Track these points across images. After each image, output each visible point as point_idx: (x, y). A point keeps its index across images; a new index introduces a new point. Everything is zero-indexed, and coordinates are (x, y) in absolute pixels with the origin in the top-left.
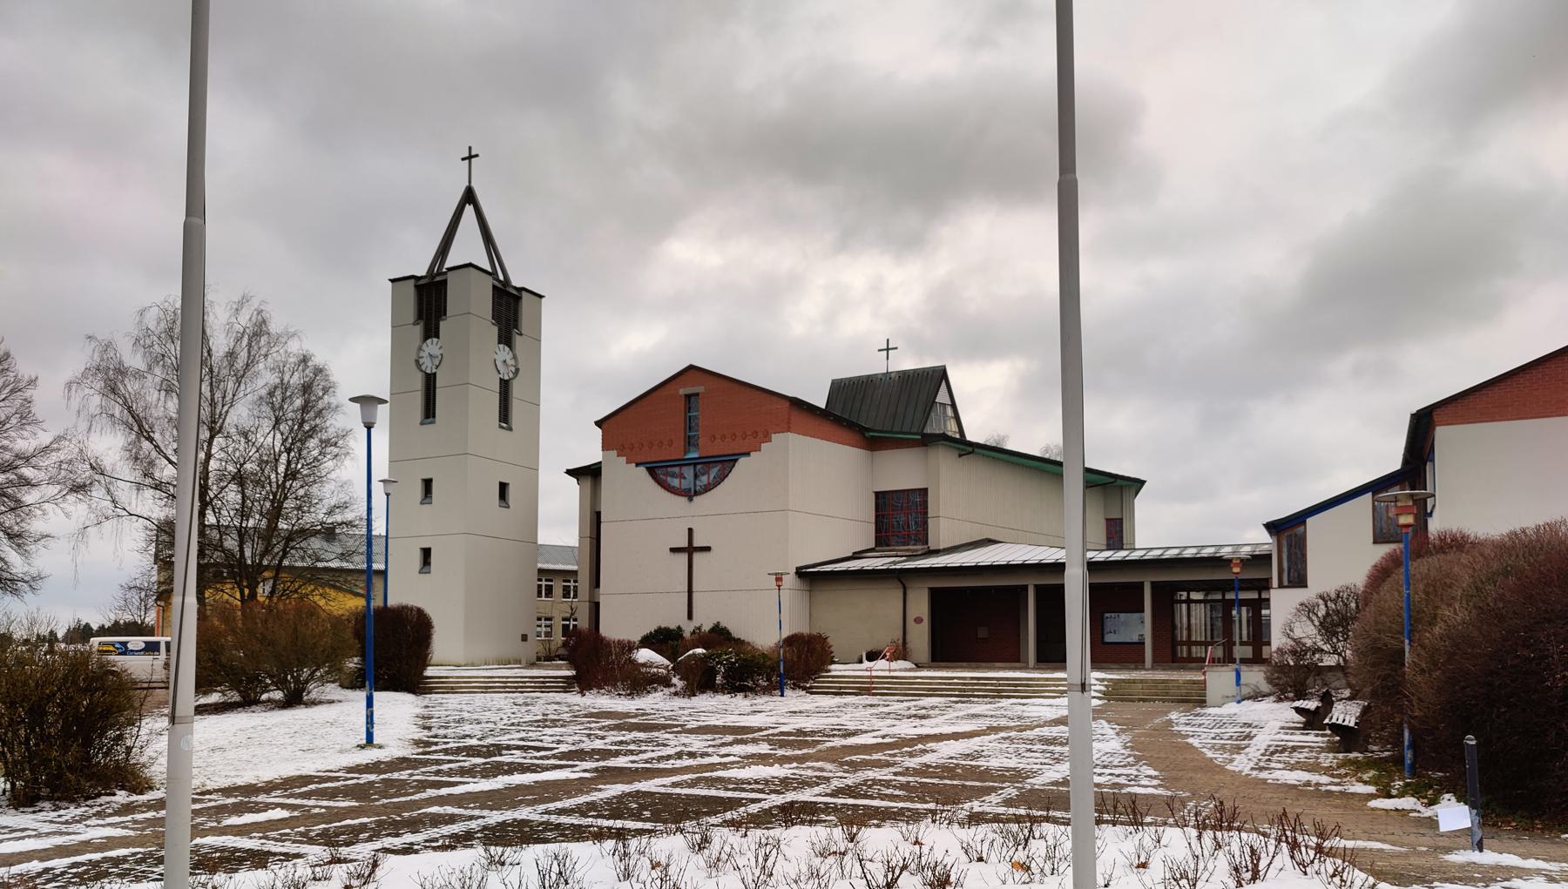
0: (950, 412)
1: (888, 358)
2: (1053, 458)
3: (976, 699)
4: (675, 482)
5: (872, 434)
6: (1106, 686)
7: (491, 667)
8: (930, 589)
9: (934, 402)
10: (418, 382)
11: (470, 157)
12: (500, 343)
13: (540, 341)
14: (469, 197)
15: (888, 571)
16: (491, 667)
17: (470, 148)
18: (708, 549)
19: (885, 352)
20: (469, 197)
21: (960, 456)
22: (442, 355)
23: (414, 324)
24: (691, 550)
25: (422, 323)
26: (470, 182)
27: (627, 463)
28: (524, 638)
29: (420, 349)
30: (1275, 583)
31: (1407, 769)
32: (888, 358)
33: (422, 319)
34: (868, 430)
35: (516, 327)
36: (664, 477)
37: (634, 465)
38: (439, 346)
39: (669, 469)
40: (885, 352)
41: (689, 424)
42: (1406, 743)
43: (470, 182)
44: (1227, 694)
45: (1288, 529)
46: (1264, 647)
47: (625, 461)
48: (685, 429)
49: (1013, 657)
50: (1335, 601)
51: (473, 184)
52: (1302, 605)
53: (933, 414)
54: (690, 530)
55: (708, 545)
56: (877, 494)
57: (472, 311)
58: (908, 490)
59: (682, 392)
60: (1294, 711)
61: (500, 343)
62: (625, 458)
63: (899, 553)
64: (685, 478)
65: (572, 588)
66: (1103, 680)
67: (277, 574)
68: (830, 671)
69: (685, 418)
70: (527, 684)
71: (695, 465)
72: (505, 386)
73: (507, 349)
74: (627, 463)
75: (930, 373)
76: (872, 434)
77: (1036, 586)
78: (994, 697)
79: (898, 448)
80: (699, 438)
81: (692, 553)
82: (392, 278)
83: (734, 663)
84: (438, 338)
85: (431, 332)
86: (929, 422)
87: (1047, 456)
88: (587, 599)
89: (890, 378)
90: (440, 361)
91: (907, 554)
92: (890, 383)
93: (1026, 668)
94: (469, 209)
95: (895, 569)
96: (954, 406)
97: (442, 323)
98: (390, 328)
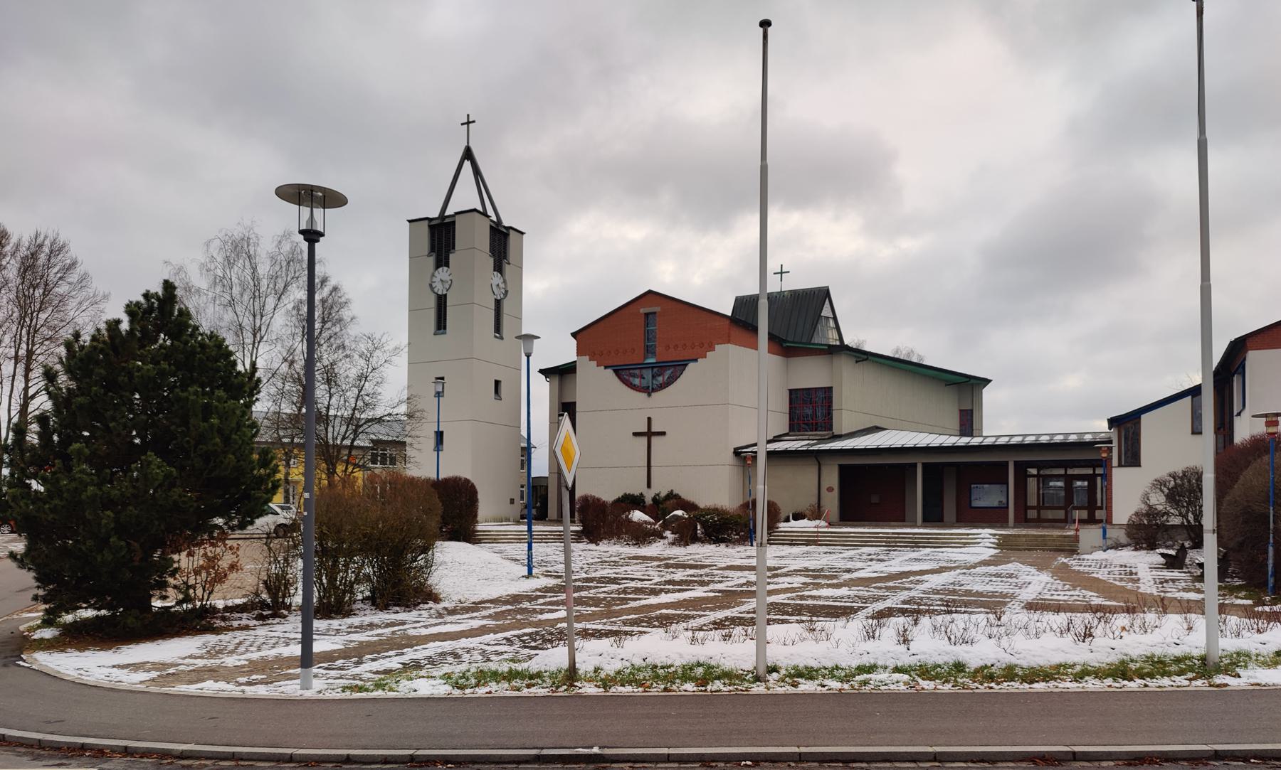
0: (832, 323)
1: (781, 280)
2: (902, 358)
3: (899, 549)
4: (637, 381)
5: (788, 344)
6: (998, 539)
7: (490, 524)
8: (1015, 461)
9: (820, 315)
10: (432, 302)
11: (468, 123)
12: (494, 270)
13: (522, 268)
14: (468, 155)
15: (807, 451)
16: (490, 524)
17: (468, 115)
18: (663, 433)
19: (780, 275)
20: (468, 155)
21: (857, 362)
22: (451, 280)
23: (428, 256)
24: (649, 434)
25: (434, 255)
26: (468, 143)
27: (598, 366)
28: (512, 501)
29: (433, 275)
30: (1115, 462)
31: (1269, 590)
32: (781, 280)
33: (434, 252)
34: (785, 341)
35: (505, 257)
36: (627, 378)
37: (603, 367)
38: (449, 272)
39: (631, 371)
40: (780, 275)
41: (648, 336)
42: (1270, 573)
43: (468, 143)
44: (1094, 545)
45: (1127, 424)
46: (1097, 511)
47: (596, 365)
48: (645, 340)
49: (900, 517)
50: (1181, 479)
51: (470, 145)
52: (1156, 480)
53: (819, 326)
54: (649, 419)
55: (663, 430)
56: (791, 391)
57: (475, 246)
58: (816, 388)
59: (642, 311)
60: (1160, 556)
61: (494, 270)
62: (596, 362)
63: (811, 437)
64: (644, 378)
65: (388, 455)
66: (995, 535)
67: (350, 452)
68: (777, 528)
69: (645, 331)
70: (549, 537)
71: (653, 368)
72: (498, 304)
73: (499, 275)
74: (598, 366)
75: (816, 293)
76: (788, 344)
77: (924, 465)
78: (912, 547)
79: (807, 355)
80: (655, 347)
81: (651, 436)
82: (410, 219)
83: (716, 521)
84: (448, 266)
85: (442, 261)
86: (815, 333)
87: (897, 356)
88: (556, 471)
89: (784, 296)
90: (450, 286)
91: (817, 438)
92: (783, 301)
93: (915, 526)
94: (467, 164)
95: (814, 450)
96: (835, 318)
97: (451, 256)
98: (408, 259)
